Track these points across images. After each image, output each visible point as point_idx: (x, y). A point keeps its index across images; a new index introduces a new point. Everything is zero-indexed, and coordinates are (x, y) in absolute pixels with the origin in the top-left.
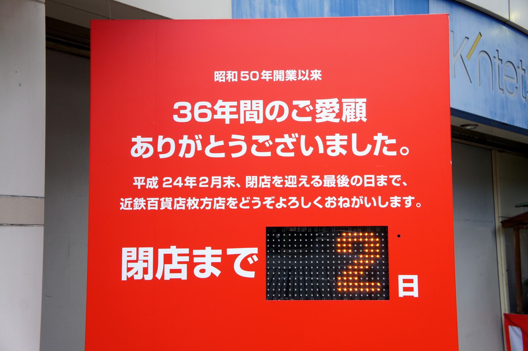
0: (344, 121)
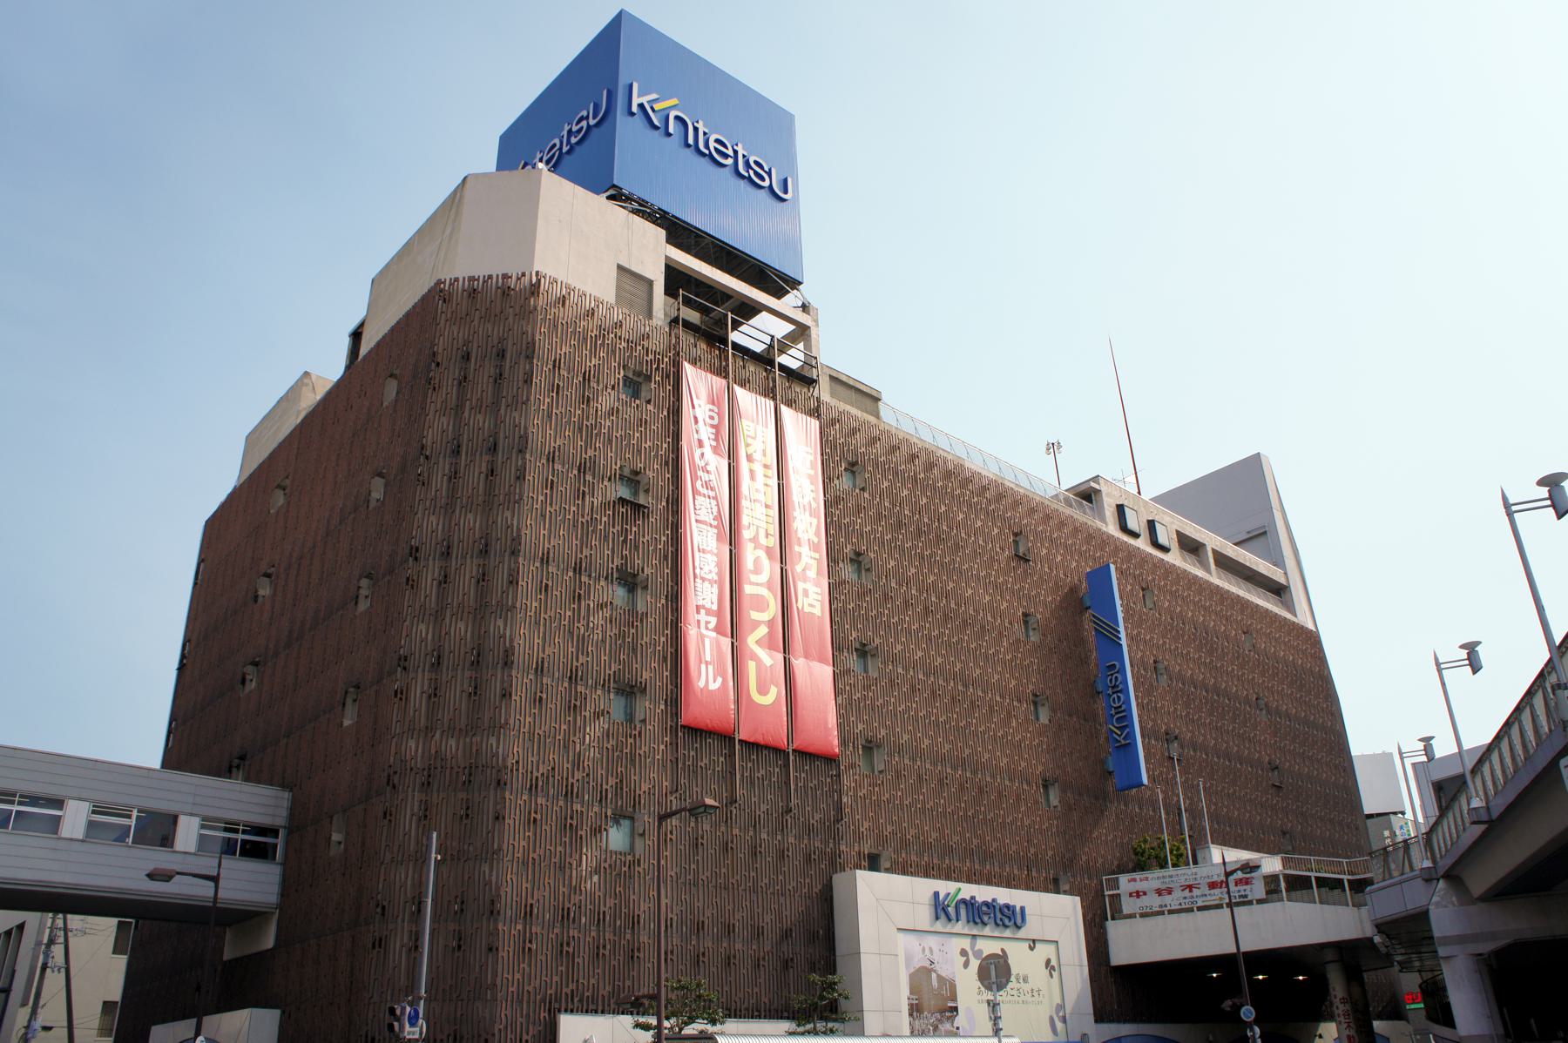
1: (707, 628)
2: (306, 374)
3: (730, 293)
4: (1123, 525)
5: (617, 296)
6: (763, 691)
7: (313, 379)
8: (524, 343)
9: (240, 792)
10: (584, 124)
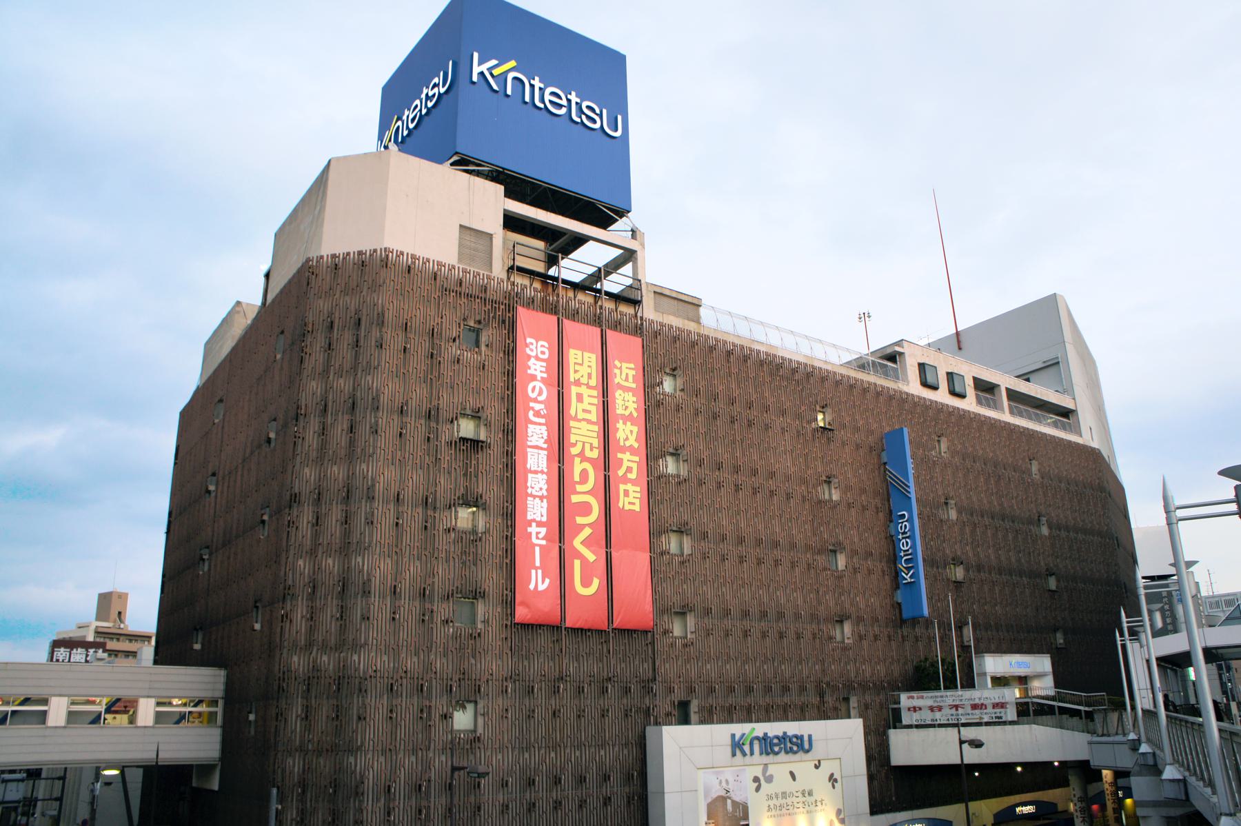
0: (574, 416)
1: (537, 538)
2: (238, 303)
3: (565, 231)
4: (924, 380)
5: (460, 254)
6: (586, 583)
7: (244, 306)
8: (376, 313)
9: (186, 675)
10: (436, 90)
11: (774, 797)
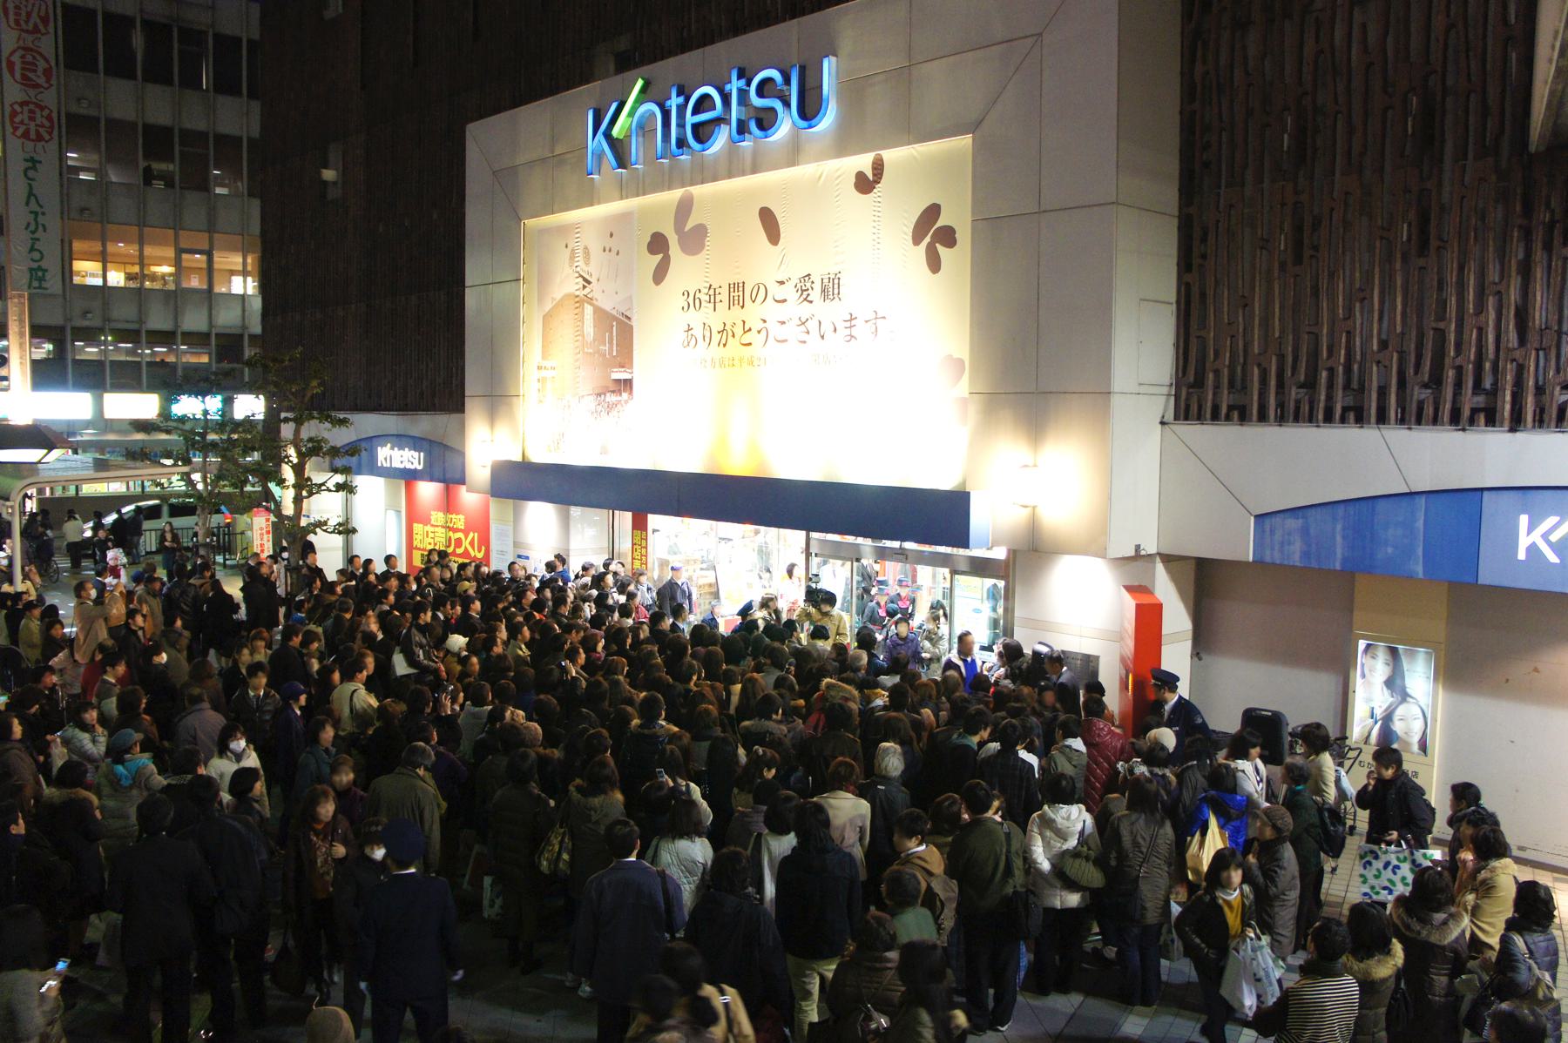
11: (705, 298)
